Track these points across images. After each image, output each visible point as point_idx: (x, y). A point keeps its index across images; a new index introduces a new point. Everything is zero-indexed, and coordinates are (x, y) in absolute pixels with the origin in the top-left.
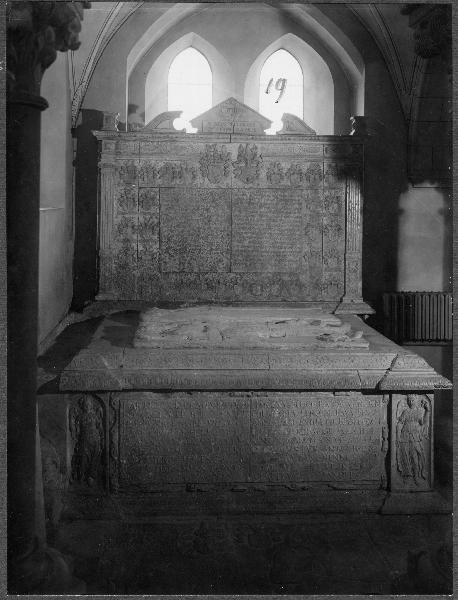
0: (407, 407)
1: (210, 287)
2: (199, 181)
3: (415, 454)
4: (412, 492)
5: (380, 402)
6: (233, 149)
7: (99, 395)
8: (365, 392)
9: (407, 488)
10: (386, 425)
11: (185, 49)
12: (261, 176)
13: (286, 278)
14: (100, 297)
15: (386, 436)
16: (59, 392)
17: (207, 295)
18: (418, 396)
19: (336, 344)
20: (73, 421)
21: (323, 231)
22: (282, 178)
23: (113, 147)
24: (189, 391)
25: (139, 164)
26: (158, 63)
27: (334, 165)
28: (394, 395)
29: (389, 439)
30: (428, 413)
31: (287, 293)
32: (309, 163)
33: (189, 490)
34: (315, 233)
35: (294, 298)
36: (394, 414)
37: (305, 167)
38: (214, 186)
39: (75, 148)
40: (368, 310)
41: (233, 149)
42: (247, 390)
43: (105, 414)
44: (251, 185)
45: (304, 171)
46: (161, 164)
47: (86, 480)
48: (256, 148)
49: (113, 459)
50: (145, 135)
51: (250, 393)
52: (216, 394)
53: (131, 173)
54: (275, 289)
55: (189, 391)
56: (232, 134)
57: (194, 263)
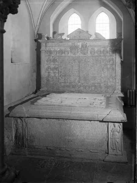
0: (114, 127)
1: (73, 87)
2: (70, 54)
3: (117, 143)
4: (115, 155)
5: (105, 125)
6: (80, 44)
7: (21, 119)
8: (100, 121)
9: (114, 153)
10: (107, 132)
11: (73, 13)
12: (88, 53)
13: (96, 85)
14: (40, 90)
15: (107, 136)
16: (9, 117)
17: (73, 89)
18: (117, 124)
19: (94, 106)
20: (14, 126)
21: (108, 69)
22: (95, 53)
23: (44, 44)
24: (47, 118)
25: (52, 50)
26: (63, 18)
27: (111, 48)
28: (109, 123)
29: (108, 137)
30: (121, 130)
31: (95, 90)
32: (103, 48)
33: (47, 149)
34: (105, 70)
35: (99, 91)
36: (109, 130)
37: (102, 49)
38: (74, 56)
39: (36, 45)
40: (122, 95)
41: (80, 44)
42: (64, 119)
43: (23, 124)
44: (85, 55)
45: (102, 51)
46: (59, 49)
47: (18, 143)
48: (87, 44)
49: (26, 138)
50: (53, 41)
51: (64, 120)
52: (55, 120)
53: (50, 52)
54: (93, 88)
55: (47, 118)
56: (80, 40)
57: (68, 80)
